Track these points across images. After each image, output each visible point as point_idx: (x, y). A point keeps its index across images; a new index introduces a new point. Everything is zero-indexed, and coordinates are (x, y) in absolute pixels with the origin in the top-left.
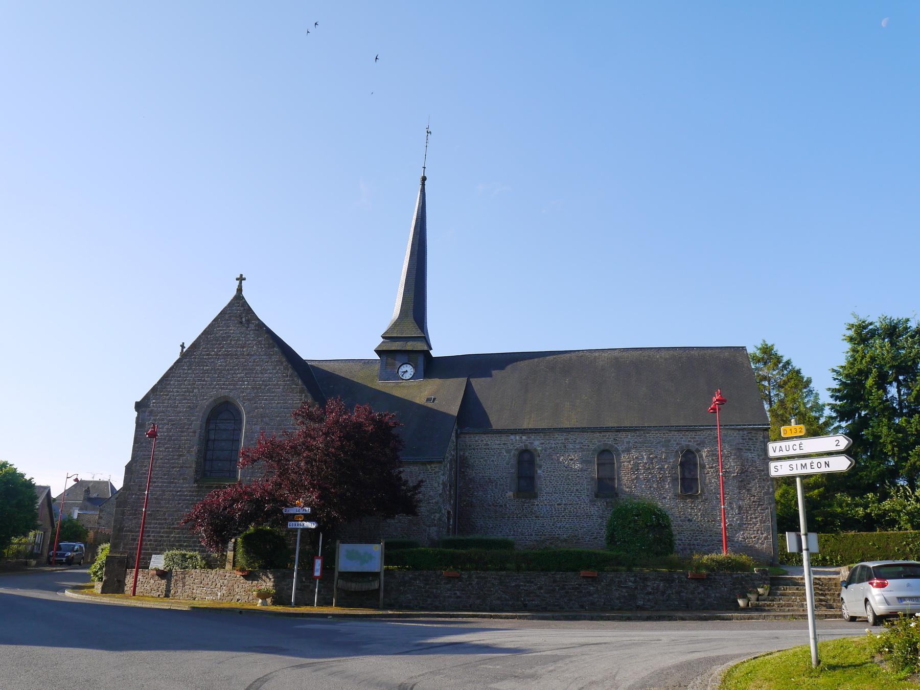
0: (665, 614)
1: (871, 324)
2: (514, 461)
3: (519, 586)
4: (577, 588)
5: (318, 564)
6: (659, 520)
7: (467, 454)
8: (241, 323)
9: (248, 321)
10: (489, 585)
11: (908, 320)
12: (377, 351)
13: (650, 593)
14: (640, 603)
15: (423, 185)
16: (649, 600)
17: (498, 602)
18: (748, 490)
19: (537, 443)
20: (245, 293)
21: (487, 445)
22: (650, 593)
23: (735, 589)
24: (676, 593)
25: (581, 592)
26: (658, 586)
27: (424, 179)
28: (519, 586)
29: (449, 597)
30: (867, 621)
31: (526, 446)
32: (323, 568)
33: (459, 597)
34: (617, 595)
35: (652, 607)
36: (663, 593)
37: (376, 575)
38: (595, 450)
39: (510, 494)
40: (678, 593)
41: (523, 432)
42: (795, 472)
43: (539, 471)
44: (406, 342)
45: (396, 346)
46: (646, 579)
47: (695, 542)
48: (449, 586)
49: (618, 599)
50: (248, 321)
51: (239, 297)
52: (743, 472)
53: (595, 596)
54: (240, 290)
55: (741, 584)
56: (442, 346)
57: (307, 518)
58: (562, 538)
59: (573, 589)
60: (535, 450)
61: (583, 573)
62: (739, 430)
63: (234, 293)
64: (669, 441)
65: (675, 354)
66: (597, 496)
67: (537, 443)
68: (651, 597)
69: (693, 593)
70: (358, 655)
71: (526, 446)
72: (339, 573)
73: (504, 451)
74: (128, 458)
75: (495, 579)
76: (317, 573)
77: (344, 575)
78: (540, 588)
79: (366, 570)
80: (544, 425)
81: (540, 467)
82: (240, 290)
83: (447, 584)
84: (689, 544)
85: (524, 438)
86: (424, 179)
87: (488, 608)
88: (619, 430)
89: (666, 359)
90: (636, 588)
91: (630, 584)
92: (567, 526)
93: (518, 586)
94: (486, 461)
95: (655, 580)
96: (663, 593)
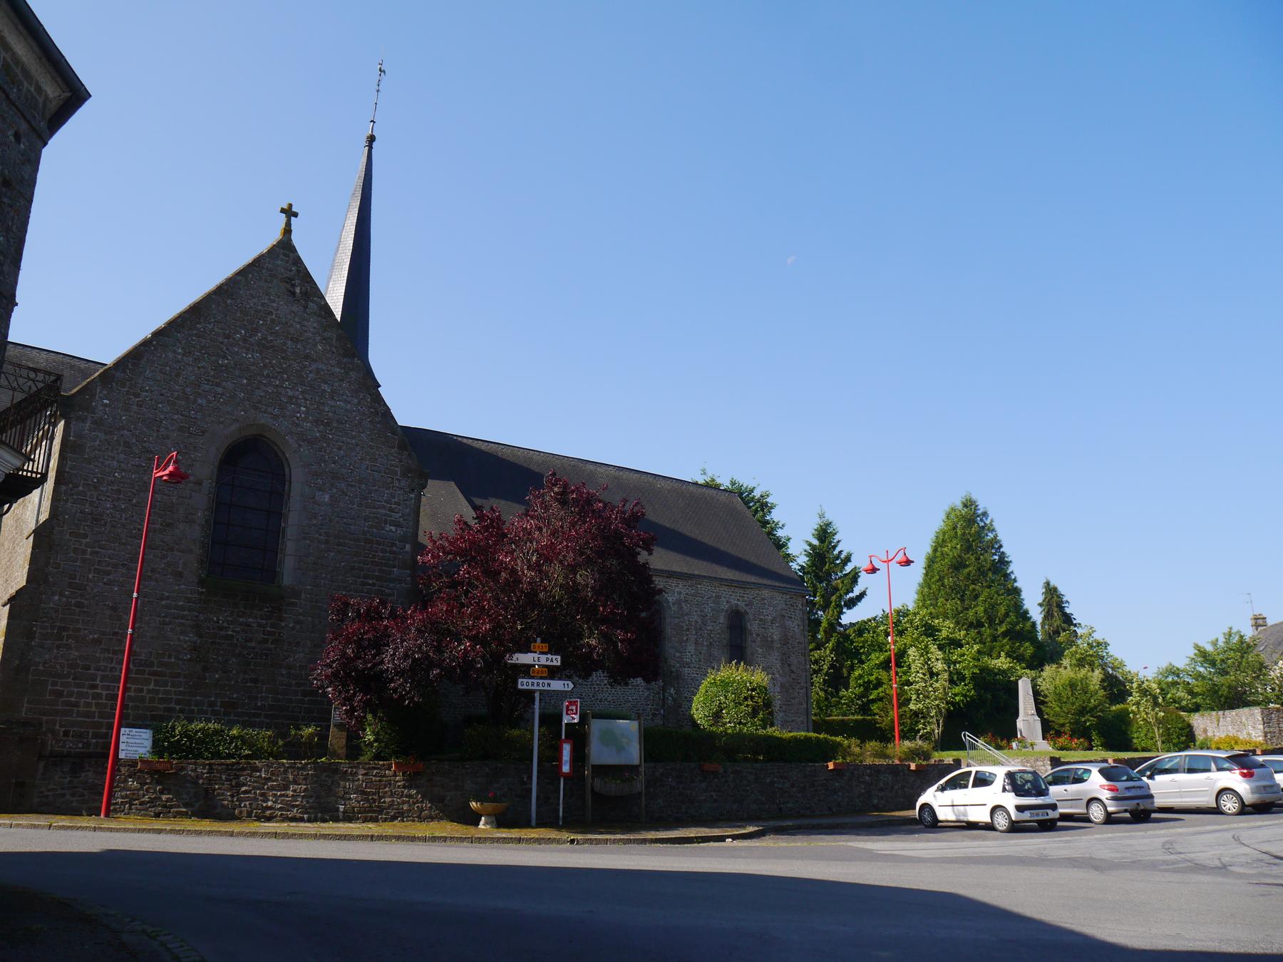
0: (824, 821)
5: (567, 750)
8: (294, 294)
20: (296, 239)
27: (372, 139)
33: (716, 801)
37: (637, 767)
42: (535, 687)
48: (704, 785)
51: (285, 247)
54: (288, 231)
57: (526, 670)
63: (275, 236)
74: (20, 579)
76: (566, 768)
77: (602, 770)
78: (793, 785)
82: (288, 231)
86: (372, 139)
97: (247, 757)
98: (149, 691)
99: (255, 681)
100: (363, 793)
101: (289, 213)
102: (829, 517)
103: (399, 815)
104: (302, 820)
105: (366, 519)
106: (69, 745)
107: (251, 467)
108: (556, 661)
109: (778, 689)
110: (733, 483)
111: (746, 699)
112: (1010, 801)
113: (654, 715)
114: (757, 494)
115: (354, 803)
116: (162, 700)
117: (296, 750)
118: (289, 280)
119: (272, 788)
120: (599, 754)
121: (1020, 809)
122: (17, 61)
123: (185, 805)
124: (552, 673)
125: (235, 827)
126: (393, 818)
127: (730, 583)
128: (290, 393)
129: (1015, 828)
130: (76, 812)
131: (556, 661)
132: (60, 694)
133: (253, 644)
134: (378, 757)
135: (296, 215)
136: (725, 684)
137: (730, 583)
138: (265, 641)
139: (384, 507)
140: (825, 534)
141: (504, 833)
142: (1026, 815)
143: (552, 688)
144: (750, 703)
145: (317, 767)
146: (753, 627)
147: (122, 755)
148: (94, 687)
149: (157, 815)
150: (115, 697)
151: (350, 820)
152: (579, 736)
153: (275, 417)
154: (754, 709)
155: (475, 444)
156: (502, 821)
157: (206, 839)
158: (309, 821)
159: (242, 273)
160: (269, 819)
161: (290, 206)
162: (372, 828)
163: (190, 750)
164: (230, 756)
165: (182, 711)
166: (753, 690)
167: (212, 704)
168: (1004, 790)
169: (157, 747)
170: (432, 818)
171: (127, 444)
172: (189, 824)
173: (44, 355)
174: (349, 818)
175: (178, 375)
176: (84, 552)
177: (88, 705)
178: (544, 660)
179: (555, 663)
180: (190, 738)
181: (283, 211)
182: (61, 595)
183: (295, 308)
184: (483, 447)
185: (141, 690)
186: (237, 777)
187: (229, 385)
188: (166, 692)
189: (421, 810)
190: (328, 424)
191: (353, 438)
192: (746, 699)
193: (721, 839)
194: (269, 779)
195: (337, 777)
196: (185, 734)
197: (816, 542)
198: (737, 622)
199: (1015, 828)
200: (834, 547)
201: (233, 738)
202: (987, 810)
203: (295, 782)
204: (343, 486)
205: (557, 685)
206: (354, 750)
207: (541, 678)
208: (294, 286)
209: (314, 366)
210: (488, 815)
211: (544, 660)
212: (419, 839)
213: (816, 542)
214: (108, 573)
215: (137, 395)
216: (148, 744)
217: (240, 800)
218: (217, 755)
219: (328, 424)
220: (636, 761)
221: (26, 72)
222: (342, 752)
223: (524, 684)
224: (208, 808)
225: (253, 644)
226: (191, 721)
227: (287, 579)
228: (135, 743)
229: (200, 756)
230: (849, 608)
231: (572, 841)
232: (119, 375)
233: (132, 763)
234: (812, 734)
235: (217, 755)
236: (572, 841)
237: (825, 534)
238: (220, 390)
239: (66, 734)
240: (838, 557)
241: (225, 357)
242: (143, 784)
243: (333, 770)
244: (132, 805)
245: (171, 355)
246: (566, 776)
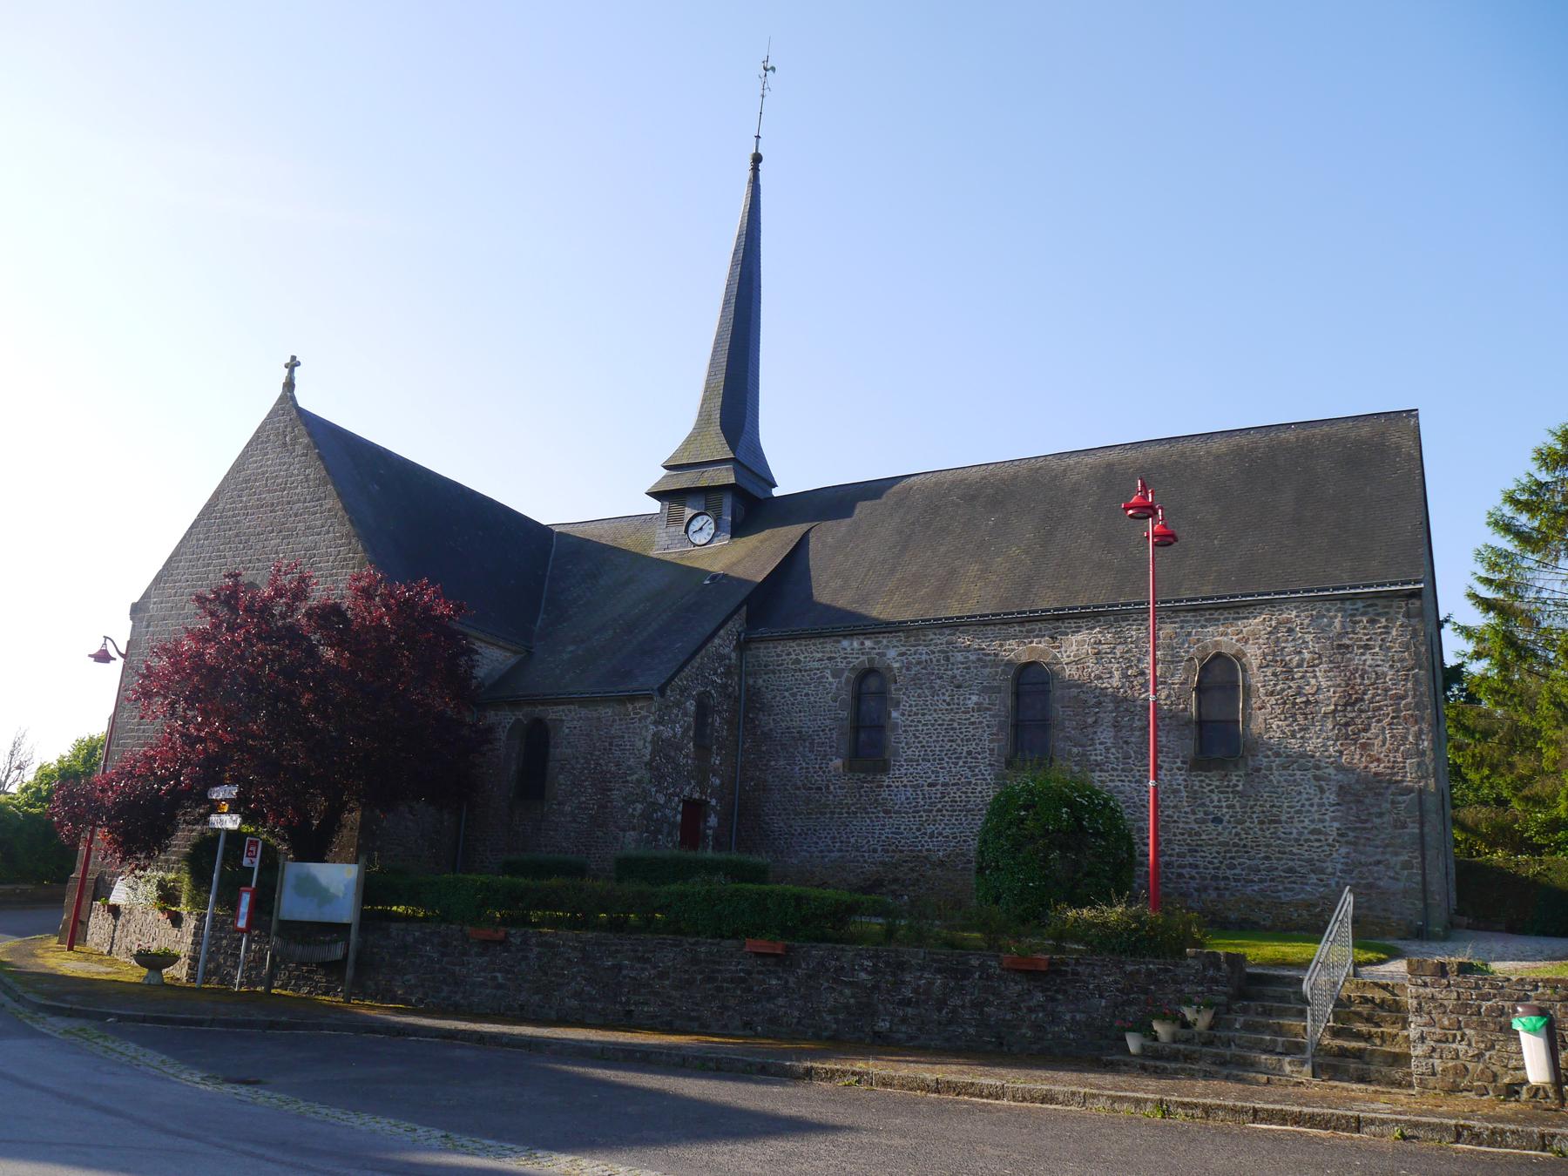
2: (846, 695)
3: (619, 967)
4: (743, 980)
6: (1079, 820)
7: (760, 681)
8: (285, 444)
10: (559, 962)
12: (656, 495)
13: (906, 1002)
14: (883, 1025)
15: (755, 170)
16: (904, 1020)
17: (574, 1003)
18: (1364, 746)
19: (892, 653)
21: (797, 661)
22: (906, 1002)
23: (1130, 1003)
24: (974, 1005)
25: (750, 990)
26: (931, 983)
27: (757, 159)
28: (619, 967)
29: (483, 984)
31: (871, 660)
33: (500, 987)
34: (831, 1002)
35: (911, 1038)
36: (941, 1004)
37: (342, 929)
39: (838, 762)
40: (978, 1005)
43: (894, 714)
44: (726, 479)
45: (685, 480)
46: (902, 966)
47: (1229, 873)
49: (830, 1012)
52: (1350, 701)
53: (780, 1001)
54: (289, 385)
55: (1146, 991)
56: (789, 479)
58: (935, 859)
59: (732, 981)
60: (890, 668)
61: (752, 945)
62: (1343, 599)
63: (277, 391)
65: (1244, 441)
66: (1009, 764)
67: (892, 653)
68: (910, 1011)
69: (1015, 1007)
70: (645, 1072)
71: (871, 660)
73: (828, 673)
75: (574, 949)
78: (662, 975)
79: (326, 918)
80: (906, 615)
81: (897, 704)
82: (289, 385)
83: (481, 955)
84: (1215, 878)
85: (868, 643)
86: (757, 159)
87: (553, 1015)
89: (1218, 457)
90: (876, 987)
91: (863, 975)
92: (947, 832)
93: (619, 968)
94: (794, 695)
95: (923, 968)
96: (941, 1004)
109: (1333, 798)
120: (292, 906)
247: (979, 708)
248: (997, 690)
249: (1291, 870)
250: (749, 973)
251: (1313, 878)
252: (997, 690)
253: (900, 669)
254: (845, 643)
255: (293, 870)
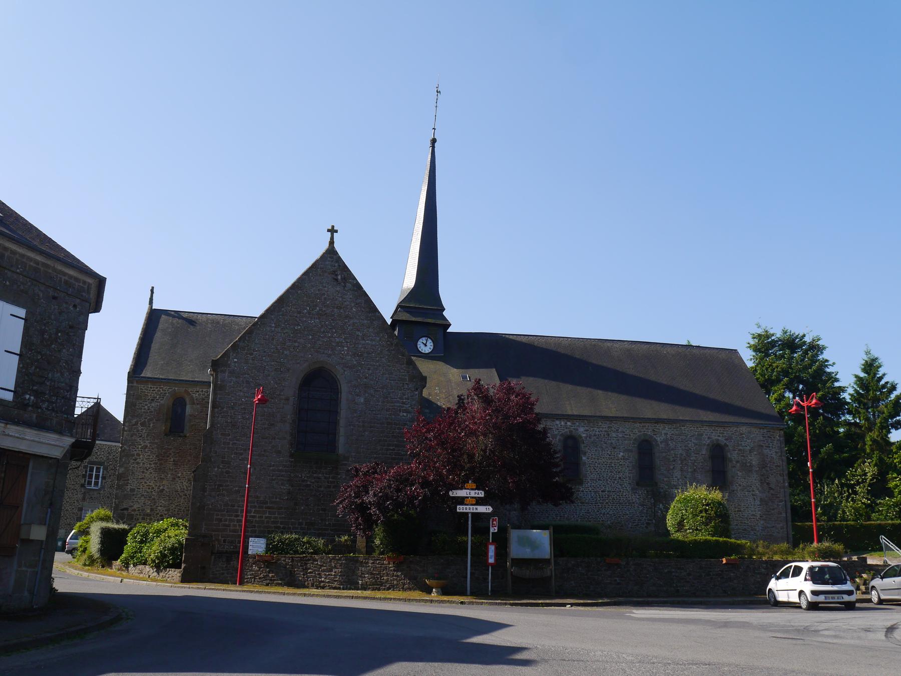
1: (773, 335)
5: (492, 549)
8: (337, 280)
9: (344, 279)
11: (804, 336)
15: (433, 147)
19: (581, 429)
20: (337, 246)
27: (434, 141)
30: (800, 607)
31: (571, 432)
32: (497, 554)
33: (618, 584)
37: (547, 561)
38: (635, 440)
41: (568, 417)
43: (584, 458)
50: (344, 279)
51: (331, 253)
54: (332, 242)
57: (461, 501)
60: (581, 437)
63: (325, 246)
64: (702, 435)
66: (638, 484)
67: (581, 429)
71: (571, 432)
72: (513, 559)
76: (491, 560)
77: (521, 562)
78: (689, 574)
79: (536, 557)
81: (585, 453)
82: (332, 242)
85: (569, 423)
86: (434, 141)
88: (658, 421)
92: (611, 512)
97: (312, 553)
98: (266, 518)
99: (324, 510)
100: (372, 574)
101: (333, 231)
102: (875, 354)
103: (392, 587)
104: (339, 588)
105: (387, 410)
106: (226, 547)
107: (318, 385)
108: (481, 494)
109: (759, 503)
110: (785, 332)
111: (701, 512)
112: (809, 587)
113: (648, 524)
114: (808, 339)
115: (367, 580)
116: (274, 522)
117: (339, 549)
118: (334, 273)
119: (323, 571)
120: (516, 550)
121: (814, 593)
122: (71, 277)
123: (281, 580)
124: (479, 502)
125: (306, 591)
126: (389, 589)
127: (710, 424)
128: (337, 340)
129: (813, 607)
130: (226, 582)
131: (481, 494)
132: (220, 520)
133: (322, 489)
134: (382, 553)
135: (336, 231)
136: (686, 501)
137: (710, 424)
138: (329, 487)
139: (398, 402)
140: (871, 366)
141: (445, 598)
142: (821, 598)
143: (478, 511)
144: (704, 514)
145: (347, 559)
146: (733, 455)
147: (250, 553)
148: (237, 516)
149: (267, 585)
150: (241, 521)
151: (365, 589)
152: (502, 541)
153: (329, 356)
154: (707, 518)
155: (518, 339)
156: (445, 591)
157: (267, 595)
158: (343, 589)
159: (306, 274)
160: (323, 588)
161: (333, 227)
162: (319, 591)
163: (283, 550)
164: (303, 553)
165: (284, 528)
166: (707, 505)
167: (300, 524)
168: (806, 580)
169: (268, 549)
170: (410, 589)
171: (248, 382)
172: (280, 589)
173: (244, 319)
174: (364, 588)
175: (273, 339)
176: (229, 444)
177: (235, 526)
178: (473, 493)
179: (480, 495)
180: (283, 543)
181: (329, 231)
182: (219, 468)
183: (338, 289)
184: (524, 340)
185: (261, 517)
186: (306, 564)
187: (302, 341)
188: (276, 518)
189: (404, 584)
190: (361, 355)
191: (378, 361)
192: (701, 512)
193: (564, 605)
194: (322, 566)
195: (358, 565)
196: (280, 541)
197: (862, 375)
198: (718, 454)
199: (813, 607)
200: (881, 378)
201: (304, 543)
202: (797, 593)
203: (335, 567)
204: (372, 391)
205: (482, 509)
206: (370, 550)
207: (472, 505)
208: (337, 275)
209: (351, 322)
210: (436, 588)
211: (473, 493)
212: (391, 599)
213: (862, 375)
214: (241, 454)
215: (252, 354)
216: (264, 546)
217: (308, 577)
218: (296, 552)
219: (361, 355)
220: (547, 556)
221: (77, 279)
222: (364, 550)
223: (460, 509)
224: (293, 582)
225: (322, 489)
226: (282, 533)
227: (341, 449)
228: (257, 546)
229: (287, 553)
230: (897, 429)
231: (462, 603)
232: (241, 344)
233: (254, 556)
234: (709, 538)
235: (296, 552)
236: (462, 603)
237: (871, 366)
238: (296, 344)
239: (224, 541)
240: (884, 386)
241: (298, 325)
242: (260, 568)
243: (355, 560)
244: (254, 579)
245: (268, 329)
246: (491, 564)
247: (624, 458)
248: (631, 451)
249: (745, 530)
250: (722, 571)
251: (752, 533)
252: (631, 451)
253: (586, 437)
254: (558, 422)
255: (514, 535)
